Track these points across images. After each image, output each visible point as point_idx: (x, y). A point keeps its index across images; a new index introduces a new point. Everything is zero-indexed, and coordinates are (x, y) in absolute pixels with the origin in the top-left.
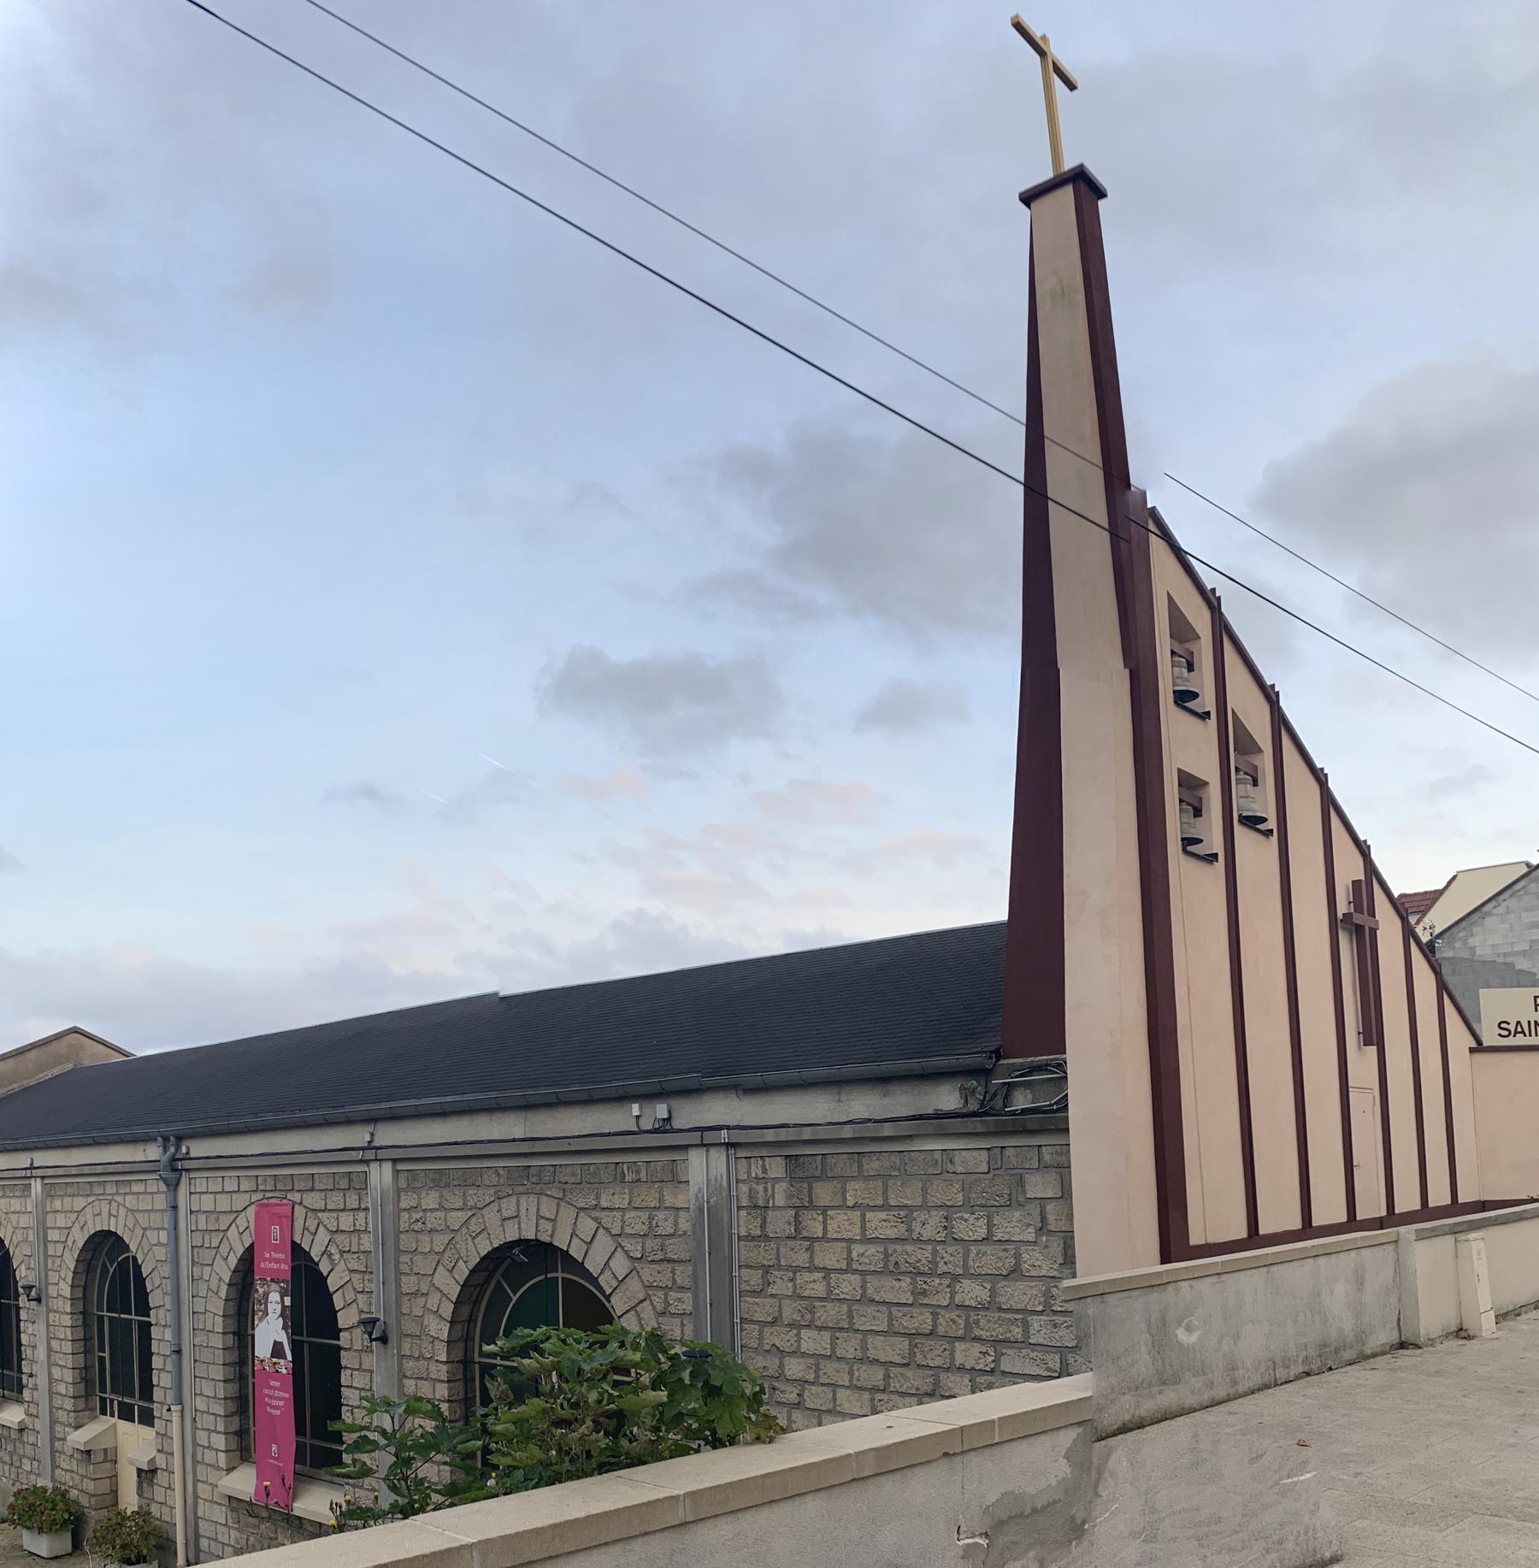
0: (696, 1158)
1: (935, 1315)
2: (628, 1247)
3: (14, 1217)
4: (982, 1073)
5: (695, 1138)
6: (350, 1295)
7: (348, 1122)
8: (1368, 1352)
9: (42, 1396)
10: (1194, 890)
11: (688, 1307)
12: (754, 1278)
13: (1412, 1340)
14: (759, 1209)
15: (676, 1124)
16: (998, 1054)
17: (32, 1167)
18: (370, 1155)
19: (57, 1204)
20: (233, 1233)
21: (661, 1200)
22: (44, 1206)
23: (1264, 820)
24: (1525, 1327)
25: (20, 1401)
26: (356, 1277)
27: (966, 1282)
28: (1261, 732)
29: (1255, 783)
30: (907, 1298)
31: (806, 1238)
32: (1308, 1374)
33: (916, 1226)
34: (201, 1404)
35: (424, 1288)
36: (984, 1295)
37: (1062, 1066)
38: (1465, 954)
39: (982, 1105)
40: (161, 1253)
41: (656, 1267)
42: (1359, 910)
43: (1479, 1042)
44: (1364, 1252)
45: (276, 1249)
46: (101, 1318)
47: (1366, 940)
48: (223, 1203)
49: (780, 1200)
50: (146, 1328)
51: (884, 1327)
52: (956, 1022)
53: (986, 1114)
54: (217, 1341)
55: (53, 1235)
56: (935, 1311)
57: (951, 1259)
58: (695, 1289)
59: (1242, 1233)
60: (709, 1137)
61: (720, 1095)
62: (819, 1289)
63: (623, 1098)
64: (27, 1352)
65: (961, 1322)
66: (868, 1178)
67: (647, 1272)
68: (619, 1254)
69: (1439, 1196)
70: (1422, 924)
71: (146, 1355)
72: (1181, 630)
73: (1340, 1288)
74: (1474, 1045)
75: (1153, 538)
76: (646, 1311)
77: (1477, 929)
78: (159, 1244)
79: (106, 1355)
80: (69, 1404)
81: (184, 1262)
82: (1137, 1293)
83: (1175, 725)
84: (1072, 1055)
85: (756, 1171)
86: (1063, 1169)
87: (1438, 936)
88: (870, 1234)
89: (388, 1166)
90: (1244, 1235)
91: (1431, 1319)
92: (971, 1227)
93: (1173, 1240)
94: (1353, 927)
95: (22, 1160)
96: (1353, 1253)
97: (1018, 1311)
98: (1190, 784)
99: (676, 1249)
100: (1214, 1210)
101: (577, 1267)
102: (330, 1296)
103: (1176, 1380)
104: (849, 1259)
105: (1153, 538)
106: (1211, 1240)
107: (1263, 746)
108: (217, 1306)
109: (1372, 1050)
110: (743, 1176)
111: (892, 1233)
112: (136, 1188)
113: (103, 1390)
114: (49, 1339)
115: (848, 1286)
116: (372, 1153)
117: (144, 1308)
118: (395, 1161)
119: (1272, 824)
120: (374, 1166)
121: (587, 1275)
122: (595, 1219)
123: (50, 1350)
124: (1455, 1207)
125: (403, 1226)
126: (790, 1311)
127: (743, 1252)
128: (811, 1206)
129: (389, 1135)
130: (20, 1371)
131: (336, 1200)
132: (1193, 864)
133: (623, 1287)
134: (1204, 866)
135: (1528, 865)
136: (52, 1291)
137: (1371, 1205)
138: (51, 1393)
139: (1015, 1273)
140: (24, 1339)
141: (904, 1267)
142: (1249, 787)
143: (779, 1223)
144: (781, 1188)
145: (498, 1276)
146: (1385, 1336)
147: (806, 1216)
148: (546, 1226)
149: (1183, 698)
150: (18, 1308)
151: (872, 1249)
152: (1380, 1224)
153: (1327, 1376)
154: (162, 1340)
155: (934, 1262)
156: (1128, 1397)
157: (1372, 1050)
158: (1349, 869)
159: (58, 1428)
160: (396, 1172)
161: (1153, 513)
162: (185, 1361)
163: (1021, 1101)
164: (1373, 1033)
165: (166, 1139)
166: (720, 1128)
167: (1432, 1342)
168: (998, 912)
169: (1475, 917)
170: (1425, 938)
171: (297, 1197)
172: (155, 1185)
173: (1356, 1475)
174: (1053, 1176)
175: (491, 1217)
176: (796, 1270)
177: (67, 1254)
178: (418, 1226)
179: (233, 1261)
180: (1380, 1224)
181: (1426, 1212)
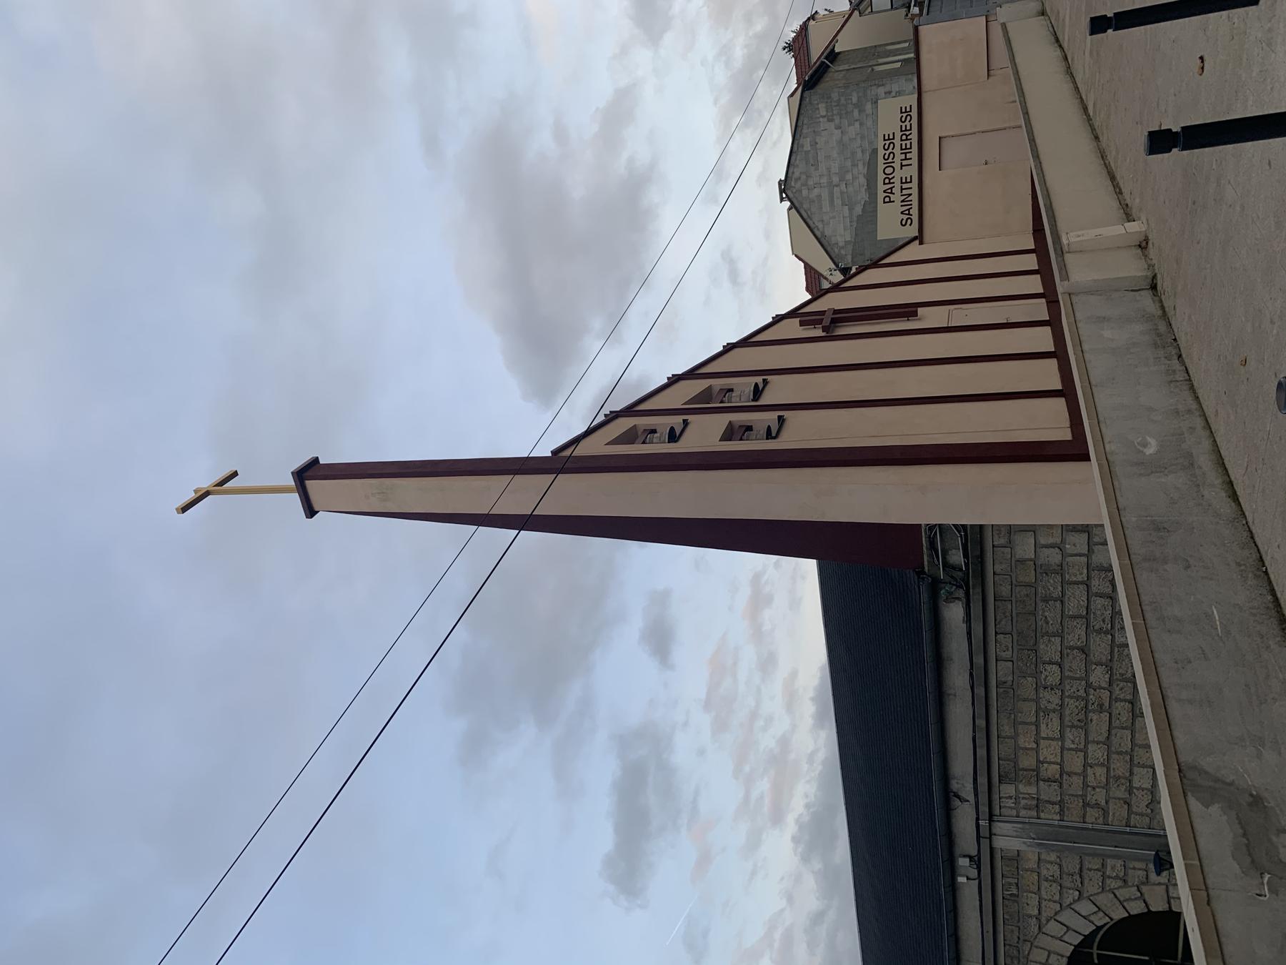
0: (1000, 843)
1: (1117, 700)
2: (1070, 900)
4: (935, 585)
5: (985, 843)
8: (1160, 312)
10: (803, 432)
13: (1149, 281)
15: (974, 853)
23: (756, 385)
24: (1137, 200)
27: (1092, 679)
28: (698, 386)
29: (732, 390)
30: (1105, 716)
31: (1061, 776)
32: (1180, 356)
33: (1050, 707)
37: (931, 528)
38: (850, 247)
39: (960, 587)
41: (1086, 882)
43: (915, 238)
47: (842, 316)
49: (1032, 790)
51: (1128, 732)
52: (898, 620)
53: (967, 585)
58: (1104, 856)
59: (1060, 403)
61: (961, 920)
62: (1100, 771)
63: (953, 887)
65: (1122, 684)
67: (1091, 888)
68: (1077, 907)
70: (830, 278)
72: (629, 437)
73: (1107, 334)
74: (917, 242)
77: (833, 240)
82: (1116, 483)
83: (690, 443)
84: (923, 522)
85: (1010, 803)
86: (1011, 530)
87: (837, 265)
88: (1057, 735)
90: (1063, 400)
92: (1051, 674)
93: (1073, 451)
96: (1079, 325)
97: (1112, 652)
98: (730, 434)
99: (1072, 864)
100: (1048, 421)
101: (1088, 940)
104: (1076, 750)
107: (708, 385)
110: (1014, 813)
111: (1056, 722)
115: (1097, 753)
119: (759, 379)
121: (1093, 934)
122: (1048, 921)
124: (1040, 250)
126: (1121, 793)
127: (1073, 818)
128: (1037, 770)
132: (785, 435)
133: (1104, 908)
135: (790, 209)
141: (1082, 716)
146: (1146, 300)
147: (1043, 774)
149: (673, 437)
151: (1069, 735)
153: (1182, 342)
156: (1206, 493)
157: (920, 310)
158: (793, 329)
161: (555, 452)
163: (957, 557)
164: (909, 311)
166: (978, 826)
167: (1151, 266)
168: (809, 567)
173: (1272, 322)
174: (1017, 538)
181: (1044, 270)
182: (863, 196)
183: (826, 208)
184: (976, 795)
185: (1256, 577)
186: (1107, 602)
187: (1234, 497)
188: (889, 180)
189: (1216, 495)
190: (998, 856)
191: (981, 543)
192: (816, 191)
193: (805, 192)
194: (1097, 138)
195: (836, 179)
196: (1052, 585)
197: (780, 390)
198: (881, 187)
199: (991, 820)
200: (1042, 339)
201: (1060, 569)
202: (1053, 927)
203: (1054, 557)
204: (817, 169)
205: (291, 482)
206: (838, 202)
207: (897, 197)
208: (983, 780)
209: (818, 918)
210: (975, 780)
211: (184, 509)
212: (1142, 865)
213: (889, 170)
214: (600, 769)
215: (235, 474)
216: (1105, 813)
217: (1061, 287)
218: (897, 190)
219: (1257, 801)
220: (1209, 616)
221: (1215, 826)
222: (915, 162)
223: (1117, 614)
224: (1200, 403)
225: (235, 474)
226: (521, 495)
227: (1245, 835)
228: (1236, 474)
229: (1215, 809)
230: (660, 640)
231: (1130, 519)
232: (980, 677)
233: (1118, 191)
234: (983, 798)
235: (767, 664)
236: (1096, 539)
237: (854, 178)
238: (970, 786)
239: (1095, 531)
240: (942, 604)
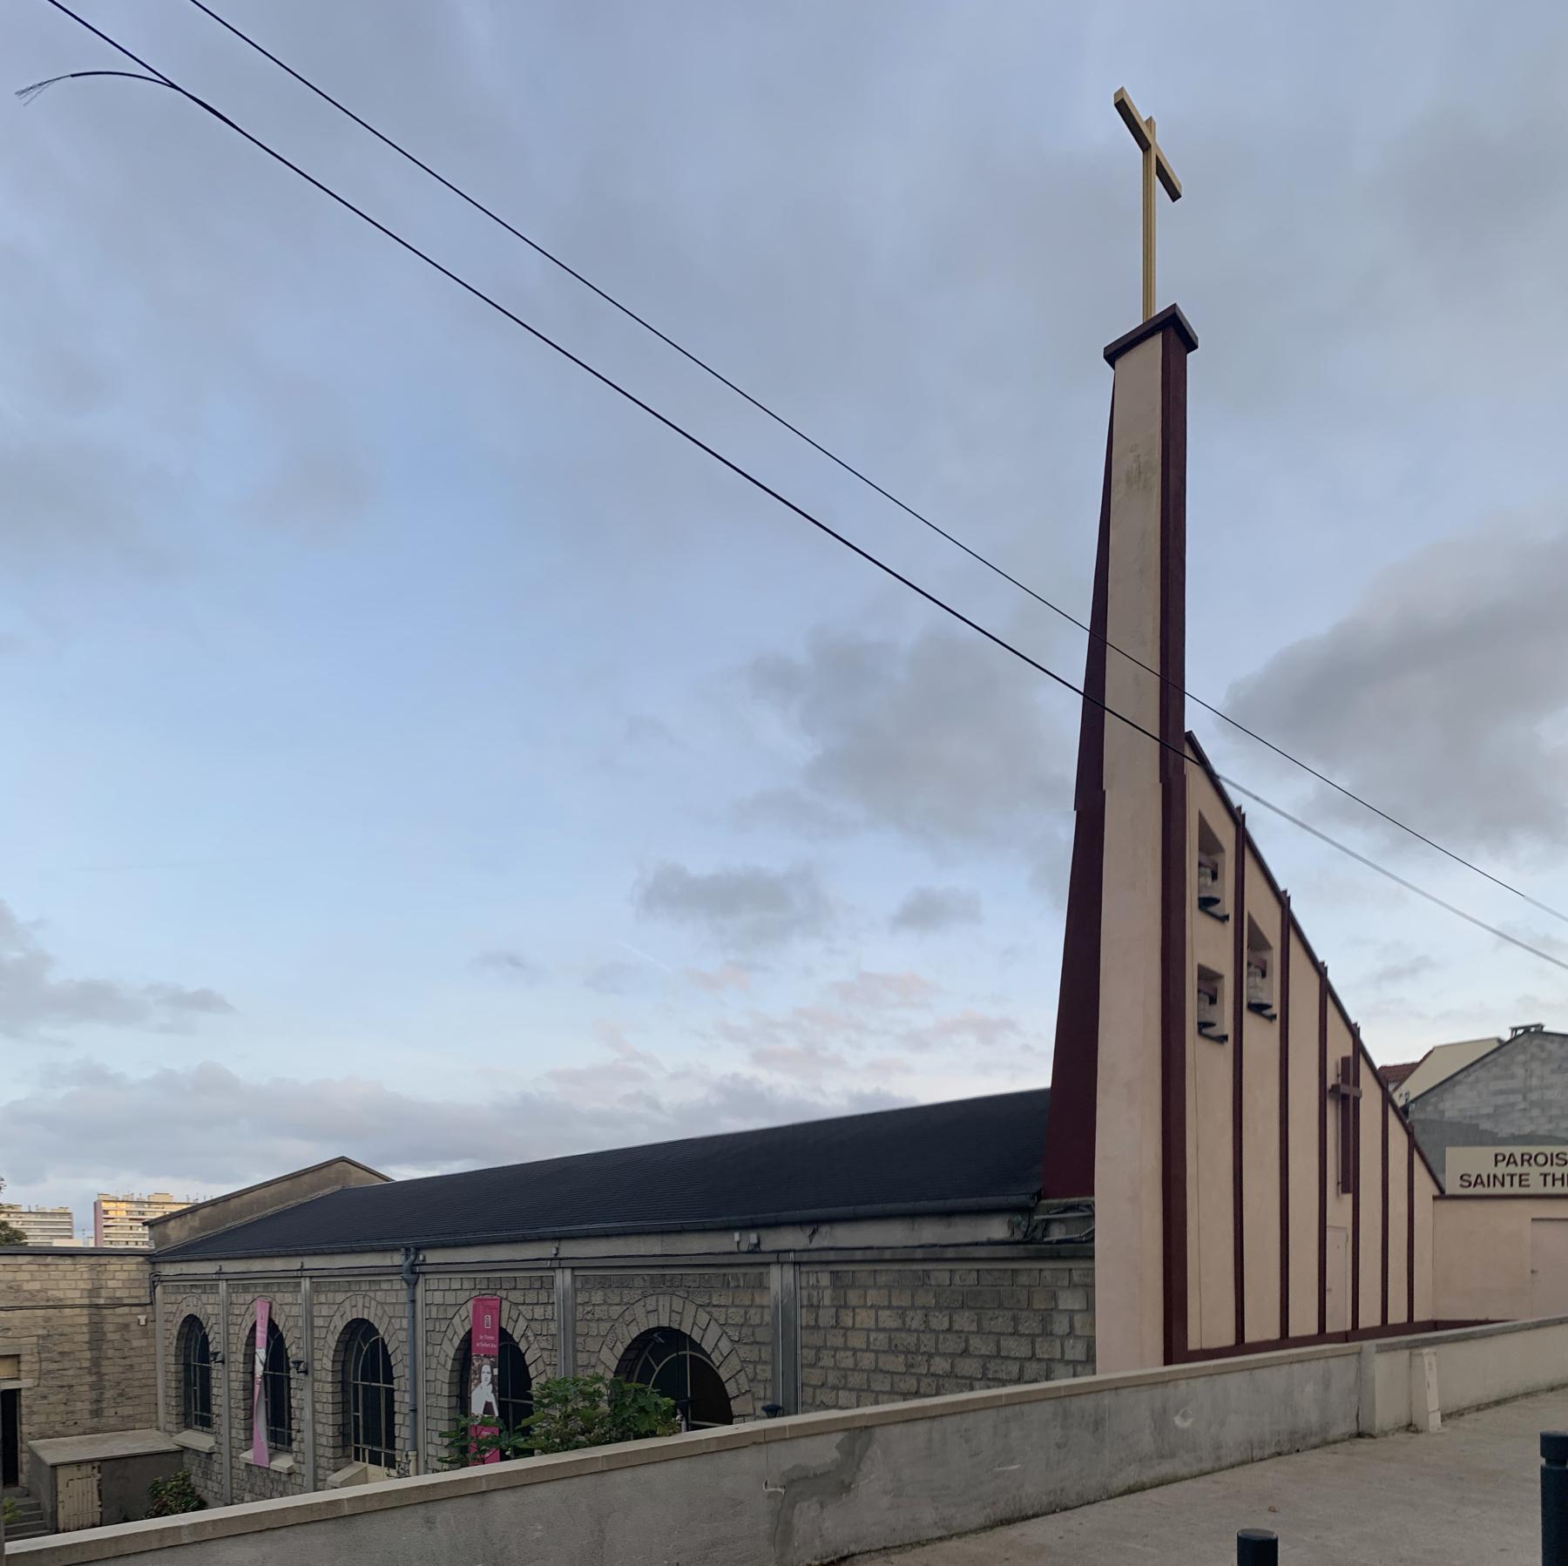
0: (775, 1272)
3: (287, 1308)
4: (1027, 1211)
5: (773, 1258)
6: (541, 1367)
7: (541, 1239)
8: (1330, 1438)
9: (307, 1446)
10: (1207, 1067)
11: (768, 1375)
12: (810, 1355)
14: (814, 1307)
16: (1040, 1196)
17: (302, 1269)
18: (555, 1264)
19: (322, 1298)
20: (456, 1320)
21: (753, 1300)
22: (311, 1299)
23: (1268, 1007)
25: (290, 1452)
26: (546, 1354)
27: (937, 1359)
30: (902, 1369)
32: (1279, 1454)
34: (431, 1450)
35: (593, 1361)
36: (947, 1367)
37: (1091, 1207)
40: (402, 1336)
42: (1348, 1079)
44: (1332, 1361)
45: (488, 1332)
46: (356, 1386)
47: (1350, 1107)
48: (450, 1298)
49: (827, 1302)
50: (390, 1392)
51: (888, 1388)
52: (999, 1173)
54: (444, 1403)
55: (318, 1322)
56: (919, 1377)
57: (928, 1343)
58: (773, 1363)
59: (1229, 1340)
60: (783, 1257)
61: (697, 1235)
62: (850, 1363)
63: (728, 1229)
64: (296, 1413)
66: (880, 1288)
67: (744, 1351)
68: (724, 1338)
69: (1397, 1315)
71: (391, 1414)
72: (1209, 843)
73: (1309, 1388)
75: (1187, 762)
76: (742, 1378)
78: (401, 1329)
79: (360, 1414)
80: (329, 1453)
81: (419, 1343)
83: (1197, 925)
85: (812, 1281)
86: (1089, 1288)
89: (568, 1273)
91: (1385, 1414)
92: (940, 1321)
93: (1175, 1347)
94: (1340, 1095)
95: (295, 1263)
97: (962, 1377)
98: (1208, 977)
99: (762, 1335)
100: (1209, 1322)
101: (696, 1346)
102: (526, 1367)
103: (1173, 1455)
105: (1188, 763)
106: (1205, 1346)
107: (1274, 946)
108: (444, 1375)
109: (1349, 1197)
112: (385, 1286)
113: (357, 1441)
114: (314, 1403)
115: (867, 1360)
116: (558, 1262)
117: (389, 1378)
118: (573, 1269)
119: (1276, 1010)
120: (559, 1273)
121: (703, 1352)
123: (314, 1411)
125: (579, 1316)
128: (846, 1306)
129: (569, 1249)
130: (290, 1428)
131: (531, 1297)
134: (1216, 1046)
135: (1499, 1040)
136: (317, 1365)
137: (1339, 1320)
138: (315, 1444)
139: (965, 1352)
140: (294, 1403)
141: (900, 1348)
142: (1258, 979)
143: (826, 1317)
144: (828, 1294)
145: (646, 1353)
146: (1345, 1427)
147: (842, 1312)
148: (676, 1317)
149: (1206, 903)
150: (289, 1379)
151: (881, 1336)
152: (1345, 1337)
153: (1295, 1457)
154: (402, 1401)
155: (918, 1345)
157: (1349, 1197)
158: (1340, 1047)
159: (320, 1472)
160: (574, 1277)
161: (1190, 739)
162: (420, 1417)
163: (1057, 1233)
164: (1350, 1183)
165: (408, 1250)
166: (789, 1251)
167: (1385, 1434)
168: (1041, 1079)
169: (1446, 1085)
170: (1400, 1103)
171: (503, 1294)
172: (399, 1284)
174: (1080, 1293)
175: (639, 1310)
176: (836, 1349)
177: (330, 1337)
178: (589, 1317)
179: (457, 1342)
180: (1345, 1337)
181: (1385, 1329)
182: (1505, 1130)
183: (1502, 1085)
184: (818, 1250)
185: (1050, 1504)
186: (1015, 1375)
187: (1130, 1491)
188: (1527, 1159)
189: (1131, 1475)
190: (762, 1270)
191: (1073, 1257)
192: (1520, 1072)
193: (1521, 1058)
194: (1552, 1389)
195: (1534, 1096)
196: (1030, 1325)
197: (1260, 1036)
198: (1518, 1151)
199: (795, 1263)
200: (1303, 1322)
201: (1047, 1333)
202: (703, 1318)
203: (1061, 1326)
204: (1553, 1072)
205: (1159, 308)
206: (1500, 1100)
207: (1502, 1169)
208: (831, 1256)
209: (655, 1105)
210: (832, 1249)
211: (1123, 107)
212: (769, 1394)
213: (1541, 1159)
214: (772, 852)
215: (1174, 195)
216: (812, 1366)
217: (1369, 1345)
218: (1512, 1169)
219: (846, 1488)
220: (1012, 1462)
221: (824, 1452)
222: (1549, 1190)
223: (1004, 1383)
224: (1227, 1468)
225: (1174, 195)
226: (1133, 691)
227: (816, 1476)
228: (1152, 1495)
229: (835, 1454)
230: (923, 913)
231: (1107, 1399)
232: (934, 1254)
233: (1479, 1408)
234: (815, 1256)
235: (917, 1041)
236: (1079, 1368)
237: (1531, 1119)
238: (826, 1244)
239: (1089, 1367)
240: (1006, 1218)
